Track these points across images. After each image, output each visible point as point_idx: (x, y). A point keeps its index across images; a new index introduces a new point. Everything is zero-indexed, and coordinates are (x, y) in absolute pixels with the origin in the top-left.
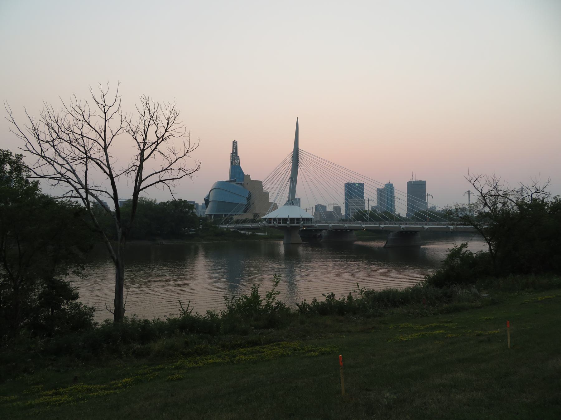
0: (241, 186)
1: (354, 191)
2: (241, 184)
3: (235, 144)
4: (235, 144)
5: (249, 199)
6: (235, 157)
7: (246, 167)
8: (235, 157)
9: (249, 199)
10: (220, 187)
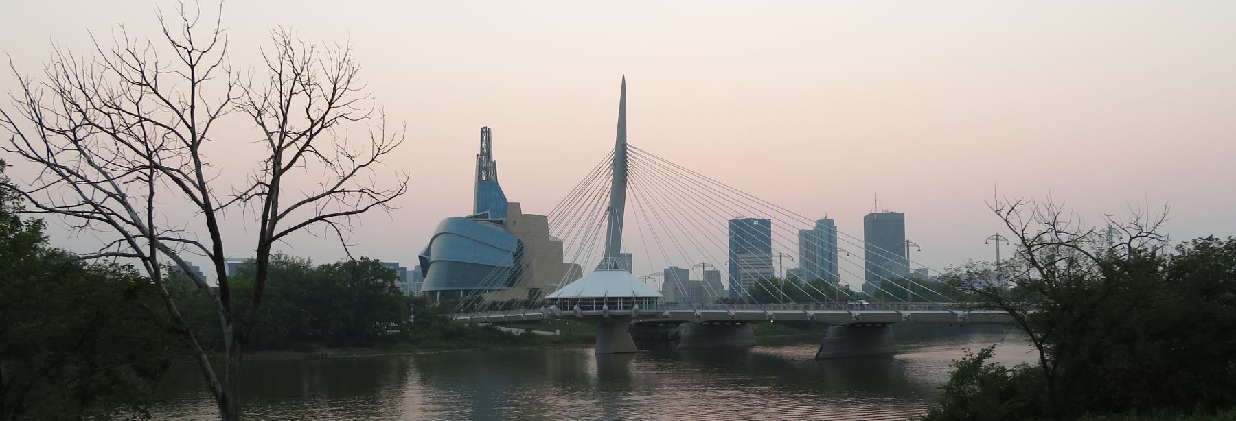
0: (500, 229)
1: (749, 236)
2: (500, 223)
3: (486, 134)
4: (486, 134)
5: (518, 255)
6: (486, 163)
7: (511, 186)
8: (486, 163)
9: (518, 255)
10: (454, 230)
